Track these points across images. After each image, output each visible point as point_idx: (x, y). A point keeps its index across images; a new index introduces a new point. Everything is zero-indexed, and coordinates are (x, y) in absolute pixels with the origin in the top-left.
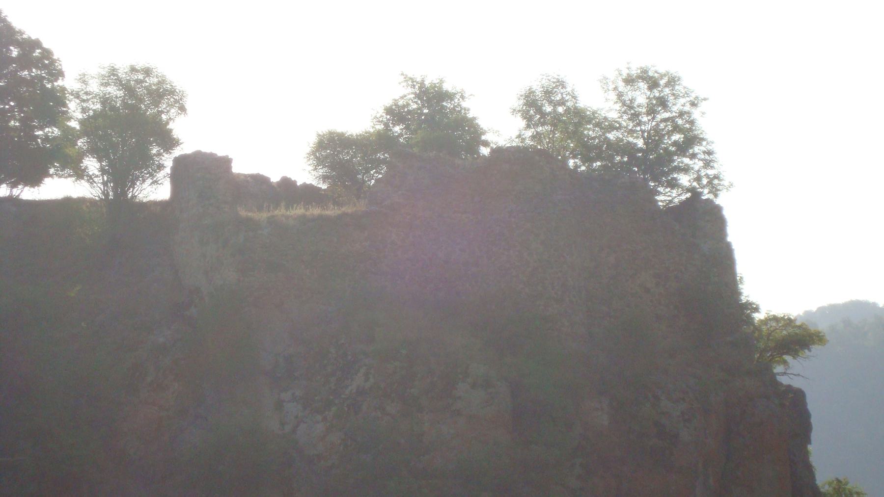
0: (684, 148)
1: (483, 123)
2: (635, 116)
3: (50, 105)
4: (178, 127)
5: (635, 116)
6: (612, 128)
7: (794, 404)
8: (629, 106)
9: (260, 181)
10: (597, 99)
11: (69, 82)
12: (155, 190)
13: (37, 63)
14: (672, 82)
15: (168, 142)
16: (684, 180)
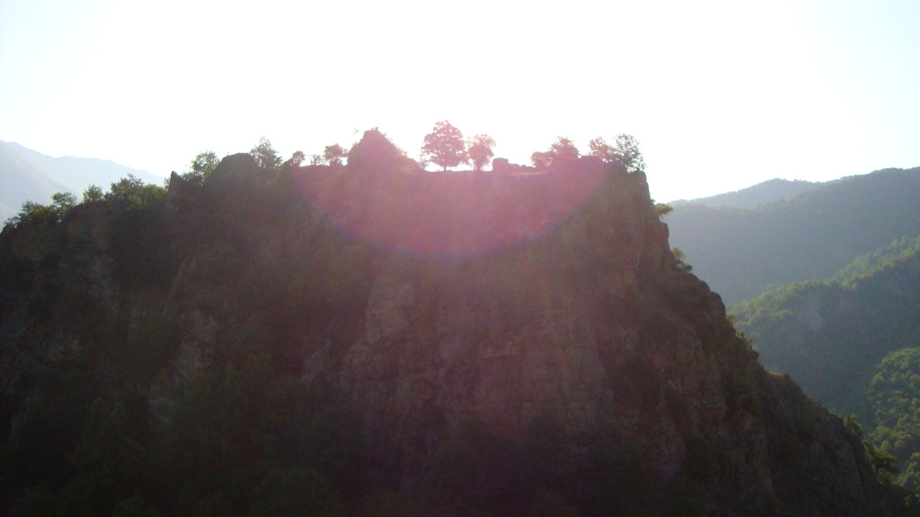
0: (635, 156)
1: (578, 149)
2: (621, 147)
3: (459, 145)
4: (494, 150)
5: (621, 147)
6: (615, 150)
7: (664, 229)
8: (620, 145)
9: (516, 165)
10: (612, 143)
11: (464, 139)
12: (488, 168)
13: (454, 133)
14: (632, 138)
15: (491, 154)
16: (635, 165)
